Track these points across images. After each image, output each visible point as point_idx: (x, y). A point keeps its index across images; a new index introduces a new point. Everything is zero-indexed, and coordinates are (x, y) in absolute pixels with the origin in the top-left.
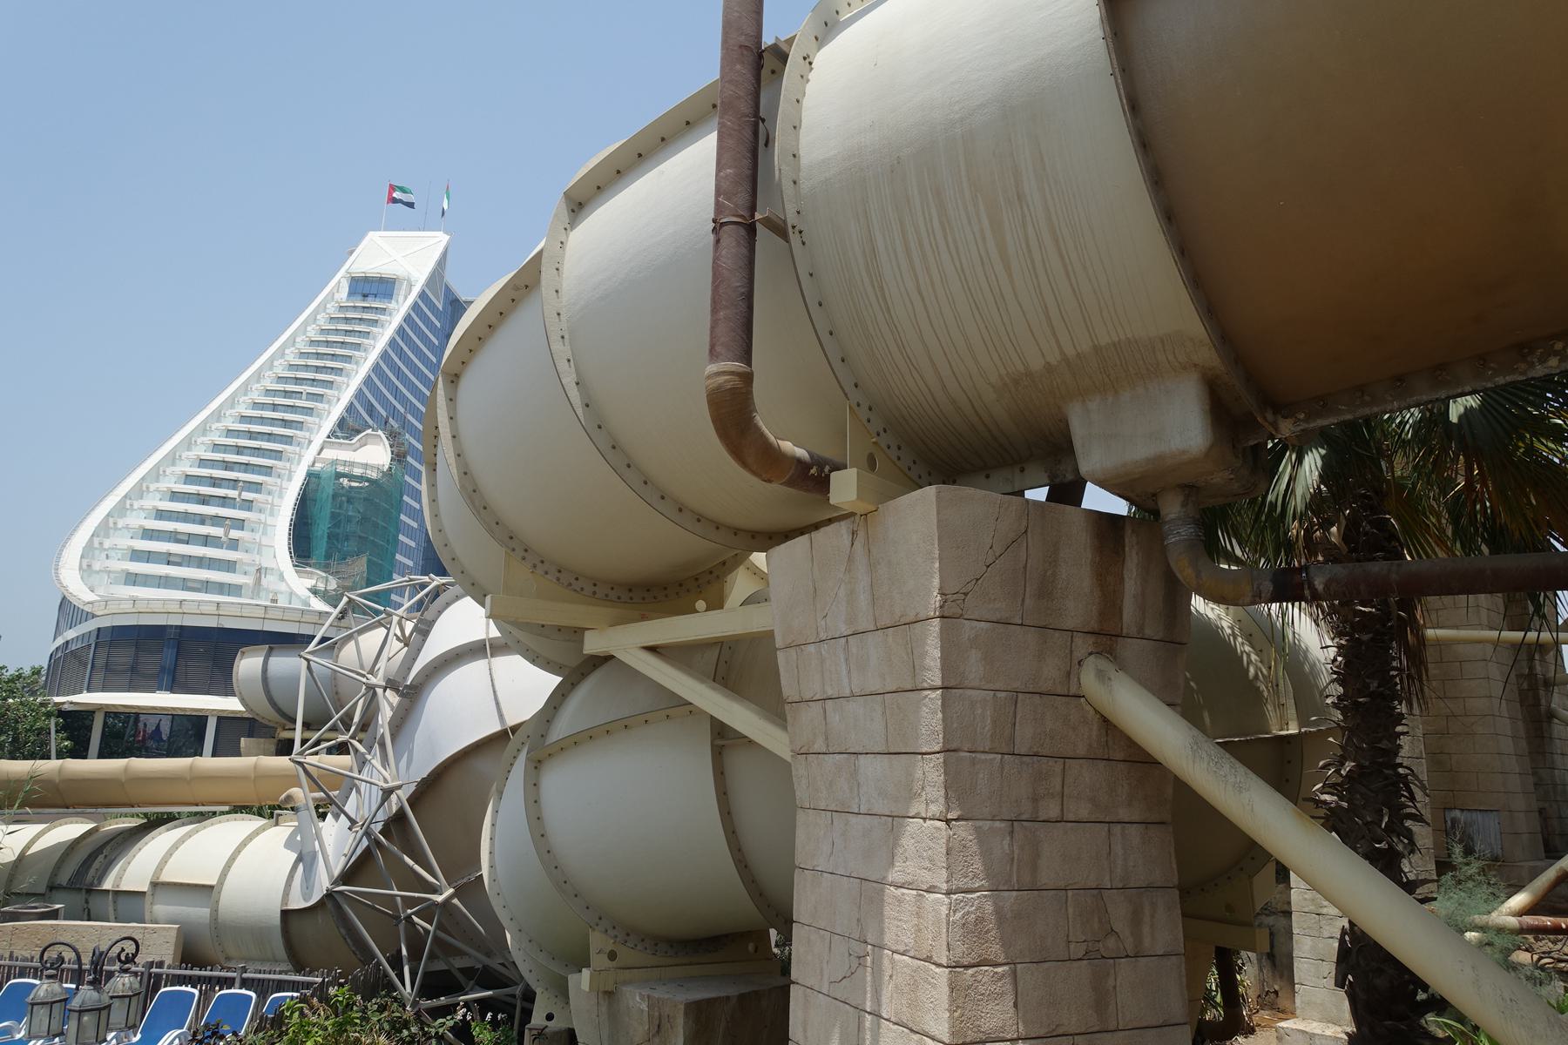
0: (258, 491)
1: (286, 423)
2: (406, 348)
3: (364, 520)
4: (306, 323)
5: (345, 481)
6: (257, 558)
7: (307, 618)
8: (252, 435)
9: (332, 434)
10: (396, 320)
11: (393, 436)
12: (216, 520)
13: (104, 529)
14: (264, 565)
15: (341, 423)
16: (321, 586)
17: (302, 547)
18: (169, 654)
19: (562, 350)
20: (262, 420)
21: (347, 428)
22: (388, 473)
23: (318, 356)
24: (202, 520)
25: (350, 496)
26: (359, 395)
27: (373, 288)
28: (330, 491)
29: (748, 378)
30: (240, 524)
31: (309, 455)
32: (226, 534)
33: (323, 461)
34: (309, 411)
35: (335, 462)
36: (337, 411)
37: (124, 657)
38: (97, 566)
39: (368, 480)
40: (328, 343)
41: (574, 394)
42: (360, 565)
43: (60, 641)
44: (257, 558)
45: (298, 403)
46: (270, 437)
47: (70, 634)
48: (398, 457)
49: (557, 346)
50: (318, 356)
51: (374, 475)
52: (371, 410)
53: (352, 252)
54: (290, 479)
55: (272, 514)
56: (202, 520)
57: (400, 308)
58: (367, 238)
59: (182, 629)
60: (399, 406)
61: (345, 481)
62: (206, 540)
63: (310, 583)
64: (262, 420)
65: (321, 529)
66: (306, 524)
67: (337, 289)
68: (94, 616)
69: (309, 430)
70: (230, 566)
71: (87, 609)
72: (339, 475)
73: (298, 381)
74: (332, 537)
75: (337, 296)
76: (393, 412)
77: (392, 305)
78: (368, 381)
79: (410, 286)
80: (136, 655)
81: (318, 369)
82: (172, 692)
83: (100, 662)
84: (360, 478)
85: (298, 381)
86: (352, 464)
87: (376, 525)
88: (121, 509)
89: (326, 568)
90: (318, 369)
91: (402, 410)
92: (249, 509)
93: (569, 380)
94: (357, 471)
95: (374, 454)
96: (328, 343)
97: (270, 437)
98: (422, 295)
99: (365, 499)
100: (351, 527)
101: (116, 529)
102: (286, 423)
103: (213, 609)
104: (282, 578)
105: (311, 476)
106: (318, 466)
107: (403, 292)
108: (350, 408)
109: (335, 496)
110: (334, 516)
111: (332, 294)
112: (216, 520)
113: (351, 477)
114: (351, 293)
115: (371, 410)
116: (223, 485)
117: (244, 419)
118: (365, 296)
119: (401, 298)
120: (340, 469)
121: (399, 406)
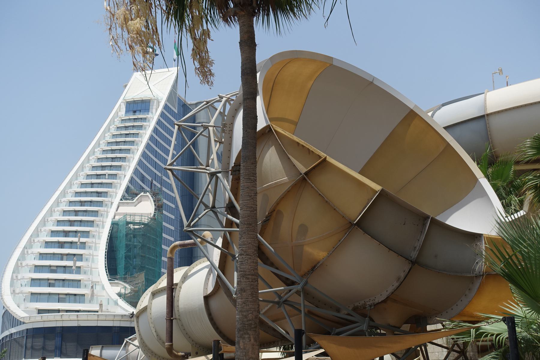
0: (88, 237)
1: (99, 194)
2: (159, 139)
3: (143, 246)
4: (104, 132)
5: (131, 226)
6: (90, 277)
7: (116, 318)
8: (82, 203)
9: (123, 198)
10: (152, 124)
11: (154, 195)
12: (69, 256)
13: (16, 270)
14: (94, 280)
15: (128, 190)
16: (123, 291)
17: (112, 271)
18: (58, 340)
19: (152, 325)
20: (86, 194)
21: (130, 194)
22: (154, 219)
23: (113, 151)
24: (61, 257)
25: (134, 234)
26: (136, 171)
27: (138, 107)
28: (124, 232)
29: (172, 345)
30: (80, 257)
31: (112, 211)
32: (75, 264)
33: (120, 214)
34: (110, 185)
35: (126, 215)
36: (125, 183)
37: (39, 342)
38: (17, 291)
39: (143, 224)
40: (117, 143)
41: (155, 334)
42: (141, 277)
43: (7, 333)
44: (90, 277)
45: (104, 181)
46: (91, 203)
47: (13, 330)
48: (159, 208)
49: (151, 325)
50: (113, 151)
51: (146, 221)
52: (143, 179)
53: (126, 86)
54: (103, 227)
55: (96, 249)
56: (61, 257)
57: (154, 117)
58: (133, 77)
59: (63, 328)
60: (158, 173)
61: (131, 226)
62: (65, 269)
63: (118, 289)
64: (86, 194)
65: (121, 253)
66: (113, 251)
67: (119, 110)
68: (24, 323)
69: (111, 196)
70: (77, 283)
71: (22, 320)
72: (128, 223)
73: (103, 167)
74: (127, 257)
75: (120, 114)
76: (155, 177)
77: (150, 115)
78: (140, 163)
79: (159, 102)
80: (44, 342)
81: (113, 159)
82: (61, 358)
83: (29, 345)
84: (139, 224)
85: (103, 167)
86: (134, 215)
87: (149, 248)
88: (23, 256)
89: (125, 280)
90: (113, 159)
91: (160, 175)
92: (84, 248)
93: (154, 331)
94: (137, 219)
95: (145, 208)
96: (117, 143)
97: (91, 203)
98: (166, 107)
99: (143, 235)
100: (136, 251)
101: (22, 267)
102: (99, 194)
103: (75, 318)
104: (103, 288)
105: (114, 225)
106: (117, 218)
107: (155, 107)
108: (132, 180)
109: (127, 235)
110: (127, 246)
111: (117, 113)
112: (69, 256)
113: (134, 224)
114: (127, 111)
115: (143, 179)
116: (68, 237)
117: (77, 194)
118: (135, 112)
119: (154, 111)
120: (128, 219)
121: (158, 173)
